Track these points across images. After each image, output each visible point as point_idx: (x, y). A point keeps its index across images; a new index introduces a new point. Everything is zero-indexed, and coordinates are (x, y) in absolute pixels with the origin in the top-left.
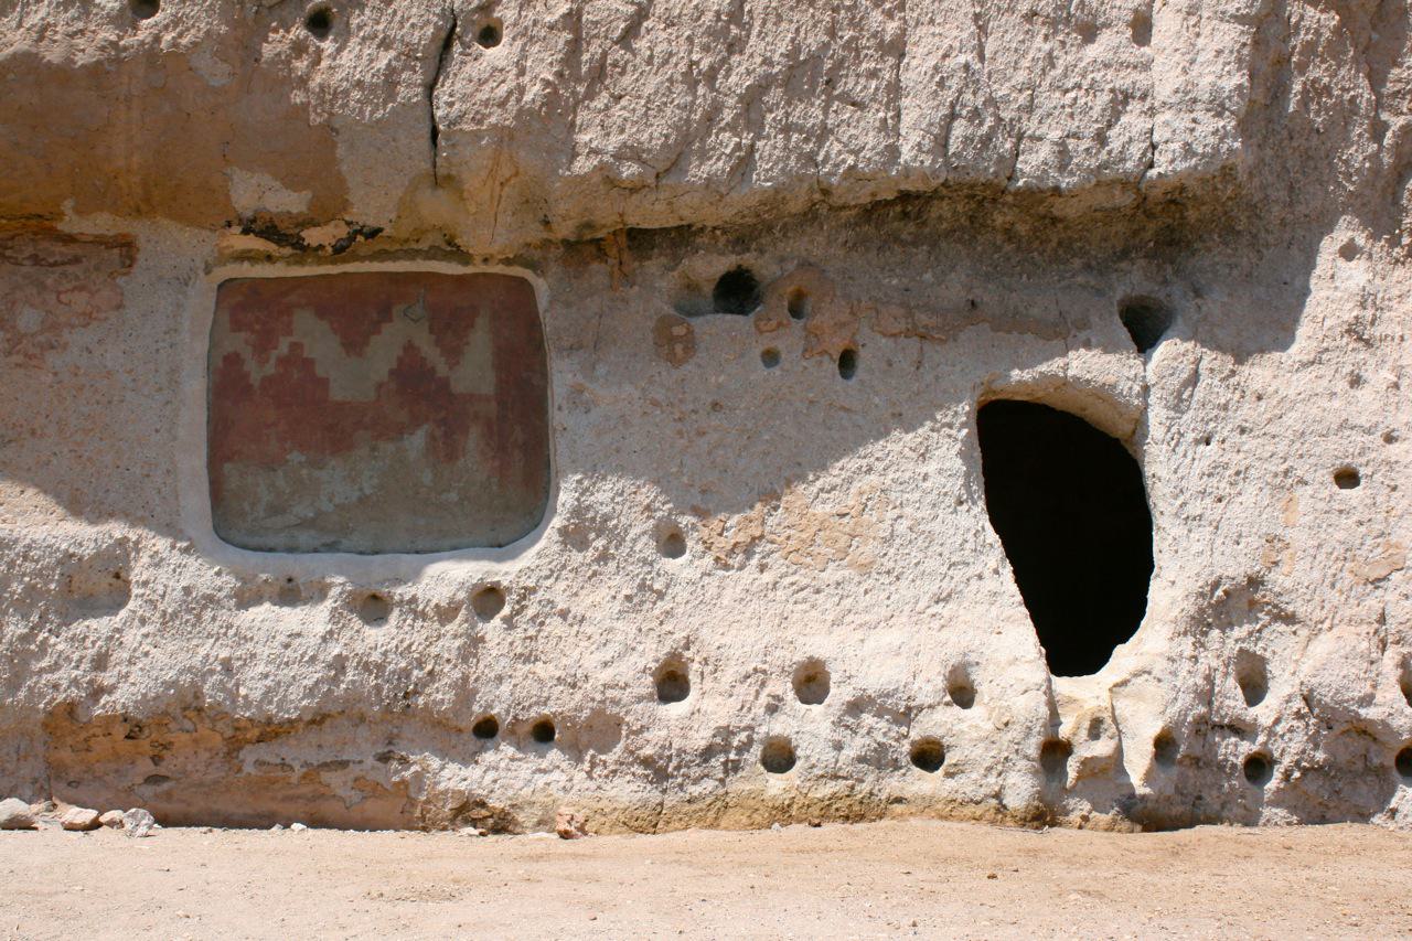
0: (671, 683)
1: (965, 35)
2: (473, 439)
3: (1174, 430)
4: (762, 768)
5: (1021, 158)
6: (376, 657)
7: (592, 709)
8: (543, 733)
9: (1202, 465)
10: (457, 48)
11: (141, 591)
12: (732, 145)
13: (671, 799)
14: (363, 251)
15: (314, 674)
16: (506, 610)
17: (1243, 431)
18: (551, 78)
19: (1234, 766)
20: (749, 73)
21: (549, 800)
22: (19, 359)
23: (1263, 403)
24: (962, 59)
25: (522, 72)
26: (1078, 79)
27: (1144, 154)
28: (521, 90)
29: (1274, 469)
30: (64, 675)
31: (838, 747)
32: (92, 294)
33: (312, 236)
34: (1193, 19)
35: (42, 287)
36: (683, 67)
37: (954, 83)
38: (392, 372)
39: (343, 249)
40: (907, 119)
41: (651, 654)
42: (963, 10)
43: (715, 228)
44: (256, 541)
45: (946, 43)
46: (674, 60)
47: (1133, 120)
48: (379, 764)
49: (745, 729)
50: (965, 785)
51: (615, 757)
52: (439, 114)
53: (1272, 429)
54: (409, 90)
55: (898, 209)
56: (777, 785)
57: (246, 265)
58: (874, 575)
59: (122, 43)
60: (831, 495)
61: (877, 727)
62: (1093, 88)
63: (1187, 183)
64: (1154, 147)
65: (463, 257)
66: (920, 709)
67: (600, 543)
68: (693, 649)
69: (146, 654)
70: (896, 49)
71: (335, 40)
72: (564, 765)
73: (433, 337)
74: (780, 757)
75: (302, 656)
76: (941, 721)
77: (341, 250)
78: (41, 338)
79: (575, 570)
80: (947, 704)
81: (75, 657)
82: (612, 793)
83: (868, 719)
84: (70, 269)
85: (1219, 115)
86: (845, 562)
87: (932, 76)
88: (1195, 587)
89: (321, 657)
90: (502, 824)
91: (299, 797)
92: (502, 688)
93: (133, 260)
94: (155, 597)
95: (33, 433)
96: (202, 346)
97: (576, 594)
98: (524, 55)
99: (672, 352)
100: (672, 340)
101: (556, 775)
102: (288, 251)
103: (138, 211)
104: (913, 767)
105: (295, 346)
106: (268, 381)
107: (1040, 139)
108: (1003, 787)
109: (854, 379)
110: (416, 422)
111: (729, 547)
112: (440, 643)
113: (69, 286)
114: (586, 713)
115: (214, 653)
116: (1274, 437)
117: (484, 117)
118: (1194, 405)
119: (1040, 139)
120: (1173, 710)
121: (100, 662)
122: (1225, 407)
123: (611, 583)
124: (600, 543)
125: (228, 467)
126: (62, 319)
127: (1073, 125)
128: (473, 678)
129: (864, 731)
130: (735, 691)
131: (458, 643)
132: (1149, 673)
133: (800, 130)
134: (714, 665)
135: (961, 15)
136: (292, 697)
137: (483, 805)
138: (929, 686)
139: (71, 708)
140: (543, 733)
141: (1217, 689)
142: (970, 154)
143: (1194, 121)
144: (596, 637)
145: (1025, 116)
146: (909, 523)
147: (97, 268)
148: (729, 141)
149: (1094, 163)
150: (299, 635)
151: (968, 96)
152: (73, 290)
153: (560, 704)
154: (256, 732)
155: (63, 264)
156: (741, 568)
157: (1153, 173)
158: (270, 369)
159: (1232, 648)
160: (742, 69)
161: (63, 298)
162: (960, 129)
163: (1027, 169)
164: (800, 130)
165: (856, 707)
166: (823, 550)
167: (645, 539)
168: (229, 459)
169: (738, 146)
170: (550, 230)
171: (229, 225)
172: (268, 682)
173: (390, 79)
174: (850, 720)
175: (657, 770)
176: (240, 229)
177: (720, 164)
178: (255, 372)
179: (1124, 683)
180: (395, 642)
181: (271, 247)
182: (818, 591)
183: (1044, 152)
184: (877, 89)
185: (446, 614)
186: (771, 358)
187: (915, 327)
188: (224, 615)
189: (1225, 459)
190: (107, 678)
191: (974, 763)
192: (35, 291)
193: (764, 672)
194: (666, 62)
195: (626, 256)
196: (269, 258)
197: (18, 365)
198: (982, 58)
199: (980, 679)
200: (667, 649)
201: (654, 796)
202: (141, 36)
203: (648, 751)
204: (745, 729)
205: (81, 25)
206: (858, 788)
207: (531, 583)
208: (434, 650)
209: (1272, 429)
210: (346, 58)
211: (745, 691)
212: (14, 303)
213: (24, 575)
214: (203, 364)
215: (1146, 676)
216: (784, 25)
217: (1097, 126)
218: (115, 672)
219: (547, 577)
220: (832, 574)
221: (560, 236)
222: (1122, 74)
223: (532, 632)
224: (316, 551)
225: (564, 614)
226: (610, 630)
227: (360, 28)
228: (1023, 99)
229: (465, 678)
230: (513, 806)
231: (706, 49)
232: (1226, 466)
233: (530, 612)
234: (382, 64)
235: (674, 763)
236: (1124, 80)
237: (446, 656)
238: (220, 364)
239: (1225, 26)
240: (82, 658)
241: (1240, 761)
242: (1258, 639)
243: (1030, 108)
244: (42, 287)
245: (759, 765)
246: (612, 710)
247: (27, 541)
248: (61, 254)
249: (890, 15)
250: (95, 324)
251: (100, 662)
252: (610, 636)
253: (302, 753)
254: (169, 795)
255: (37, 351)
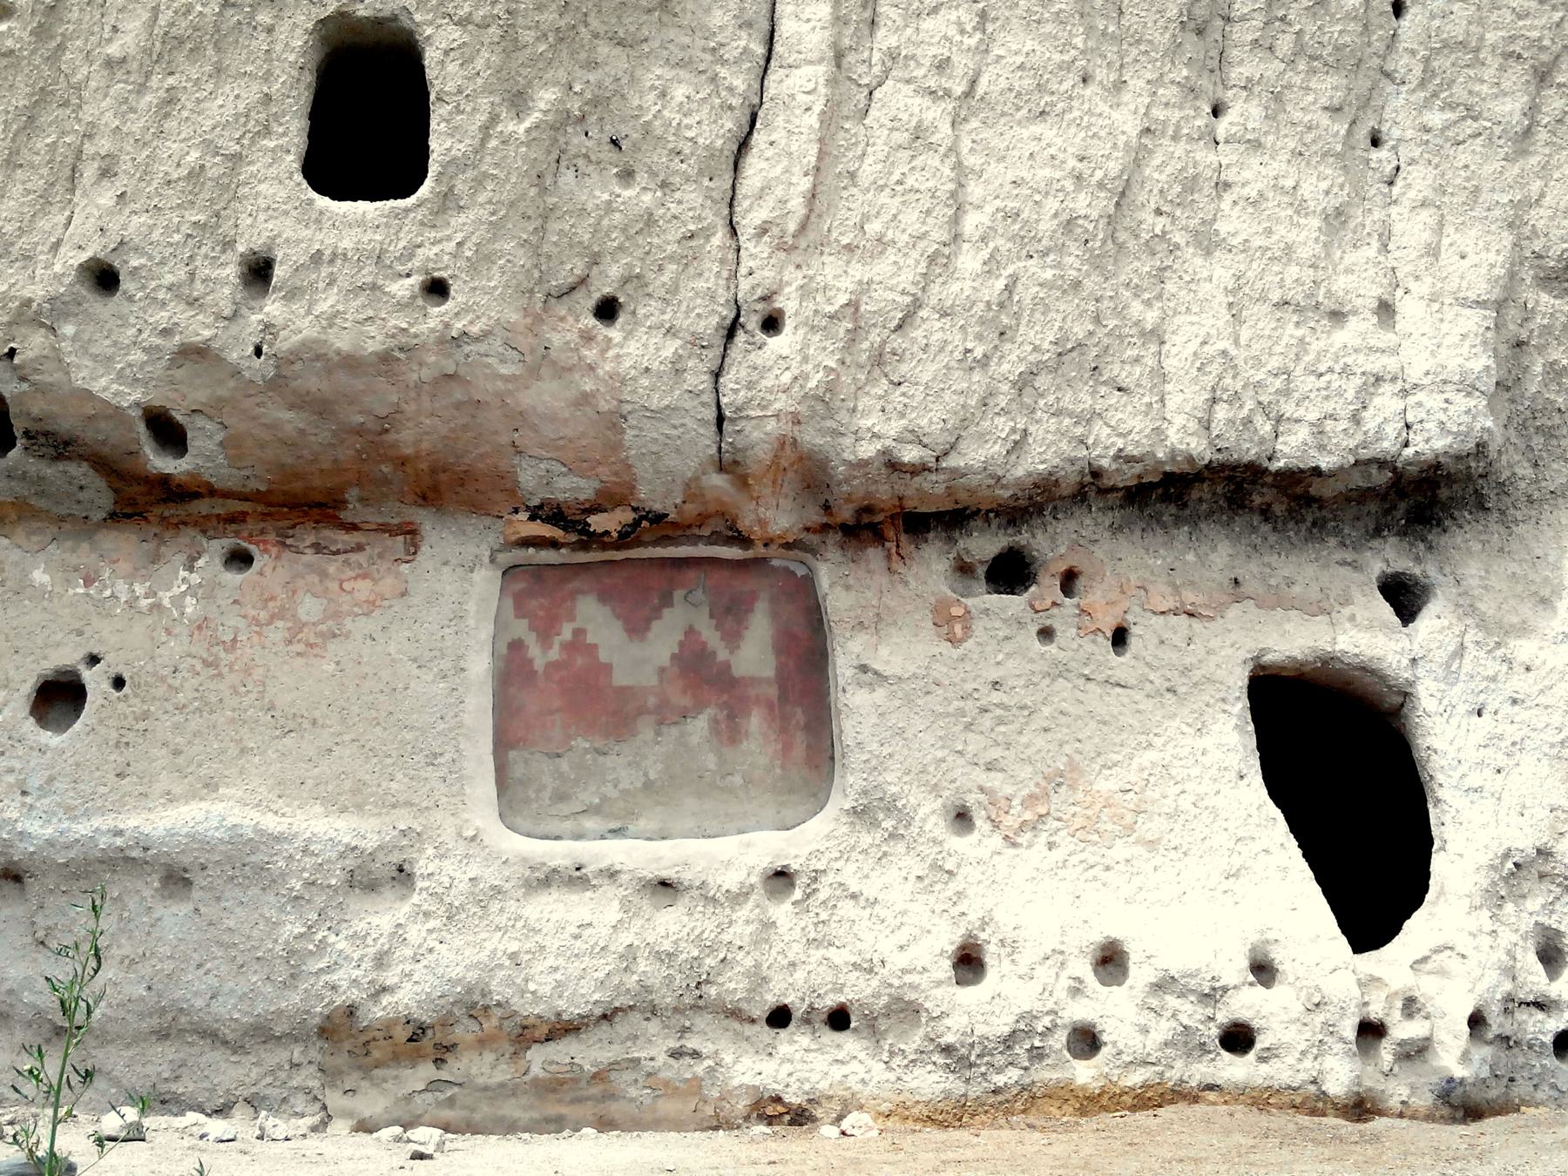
0: (969, 962)
1: (1221, 323)
2: (755, 722)
3: (1445, 702)
4: (1068, 1055)
5: (1281, 439)
6: (667, 946)
7: (889, 995)
8: (839, 1019)
9: (1479, 737)
10: (741, 337)
11: (426, 884)
12: (1007, 430)
13: (975, 1091)
14: (646, 538)
15: (604, 966)
16: (798, 894)
17: (1515, 702)
18: (834, 365)
19: (1543, 1044)
20: (1021, 360)
21: (847, 1094)
22: (300, 647)
23: (1531, 675)
24: (1221, 345)
25: (805, 359)
26: (1330, 363)
27: (1399, 434)
28: (806, 377)
29: (1551, 740)
30: (340, 977)
31: (1145, 1030)
32: (375, 581)
33: (597, 522)
34: (1436, 306)
35: (323, 575)
36: (958, 355)
37: (1215, 369)
38: (674, 657)
39: (627, 534)
40: (1171, 404)
41: (948, 939)
42: (1217, 301)
43: (988, 511)
44: (541, 829)
45: (1202, 333)
46: (950, 348)
47: (1386, 404)
48: (672, 1061)
49: (1048, 1013)
50: (1280, 1072)
51: (915, 1046)
52: (724, 400)
53: (1542, 700)
54: (698, 379)
55: (1160, 491)
56: (1085, 1073)
57: (531, 550)
58: (1162, 851)
59: (412, 330)
60: (1113, 771)
61: (1190, 1012)
62: (1346, 372)
63: (1441, 459)
64: (1408, 427)
65: (743, 541)
66: (1225, 989)
67: (888, 824)
68: (989, 930)
69: (431, 951)
70: (1156, 336)
71: (622, 329)
72: (862, 1056)
73: (714, 622)
74: (1086, 1041)
75: (593, 947)
76: (1247, 1003)
77: (627, 537)
78: (323, 627)
79: (864, 852)
80: (1251, 984)
81: (356, 956)
82: (914, 1084)
83: (1172, 1001)
84: (353, 557)
85: (1469, 394)
86: (1131, 839)
87: (1193, 363)
88: (1485, 859)
89: (612, 948)
90: (800, 1117)
91: (588, 1099)
92: (796, 976)
93: (417, 547)
94: (440, 890)
95: (314, 722)
96: (486, 631)
97: (867, 877)
98: (806, 345)
99: (951, 632)
100: (951, 619)
101: (854, 1066)
102: (573, 538)
103: (424, 498)
104: (1223, 1052)
105: (579, 633)
106: (552, 666)
107: (1298, 421)
108: (1320, 1072)
109: (1128, 655)
110: (699, 707)
111: (1017, 826)
112: (731, 930)
113: (352, 574)
114: (884, 1000)
115: (501, 947)
116: (1546, 707)
117: (770, 403)
118: (1463, 677)
119: (1298, 421)
120: (1481, 987)
121: (381, 961)
122: (1494, 679)
123: (901, 864)
124: (888, 824)
125: (512, 754)
126: (345, 607)
127: (1329, 407)
128: (765, 966)
129: (1168, 1014)
130: (1035, 973)
131: (750, 929)
132: (1451, 948)
133: (1071, 415)
134: (1011, 947)
135: (1215, 304)
136: (583, 991)
137: (778, 1100)
138: (1234, 969)
139: (351, 1011)
140: (839, 1019)
141: (1519, 965)
142: (1232, 435)
143: (1447, 401)
144: (890, 920)
145: (1282, 400)
146: (1193, 799)
147: (381, 556)
148: (1003, 425)
149: (1352, 444)
150: (590, 925)
151: (1228, 381)
152: (355, 578)
153: (856, 991)
154: (545, 1029)
155: (346, 552)
156: (1030, 846)
157: (1409, 452)
158: (555, 654)
159: (1527, 923)
160: (1013, 357)
161: (346, 586)
162: (1222, 412)
163: (1287, 450)
164: (1071, 415)
165: (1163, 985)
166: (1109, 827)
167: (933, 819)
168: (513, 748)
169: (1013, 430)
170: (831, 514)
171: (516, 511)
172: (558, 976)
173: (677, 369)
174: (1154, 1003)
175: (954, 1057)
176: (527, 515)
177: (997, 447)
178: (539, 656)
179: (1425, 959)
180: (686, 930)
181: (557, 533)
182: (1108, 869)
183: (1302, 433)
184: (1142, 375)
185: (738, 897)
186: (1046, 634)
187: (1183, 603)
188: (512, 905)
189: (1499, 731)
190: (390, 978)
191: (1289, 1046)
192: (316, 579)
193: (1062, 953)
194: (942, 350)
195: (903, 538)
196: (554, 544)
197: (299, 654)
198: (1236, 342)
199: (1278, 955)
200: (962, 931)
201: (955, 1085)
202: (432, 323)
203: (949, 1039)
204: (1048, 1013)
205: (371, 313)
206: (1167, 1075)
207: (820, 866)
208: (726, 937)
209: (1542, 700)
210: (633, 347)
211: (1044, 973)
212: (294, 592)
213: (304, 869)
214: (488, 649)
215: (1448, 952)
216: (1053, 315)
217: (1352, 407)
218: (398, 970)
219: (836, 859)
220: (1120, 850)
221: (839, 520)
222: (1372, 358)
223: (824, 916)
224: (603, 838)
225: (854, 896)
226: (904, 913)
227: (647, 317)
228: (1278, 383)
229: (757, 966)
230: (810, 1101)
231: (979, 337)
232: (1501, 737)
233: (822, 896)
234: (668, 352)
235: (977, 1050)
236: (1375, 364)
237: (739, 943)
238: (504, 651)
239: (1468, 312)
240: (363, 956)
241: (1549, 1039)
242: (1552, 912)
243: (1286, 392)
244: (323, 575)
245: (1065, 1052)
246: (910, 996)
247: (308, 835)
248: (344, 542)
249: (1148, 304)
250: (377, 613)
251: (381, 961)
252: (905, 919)
253: (586, 1053)
254: (451, 1102)
255: (319, 641)
